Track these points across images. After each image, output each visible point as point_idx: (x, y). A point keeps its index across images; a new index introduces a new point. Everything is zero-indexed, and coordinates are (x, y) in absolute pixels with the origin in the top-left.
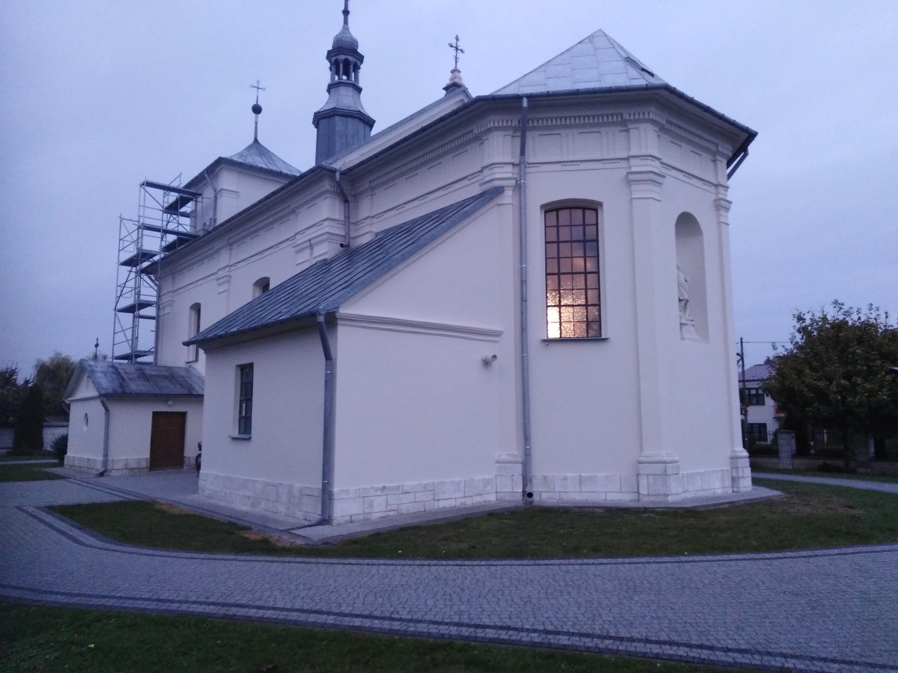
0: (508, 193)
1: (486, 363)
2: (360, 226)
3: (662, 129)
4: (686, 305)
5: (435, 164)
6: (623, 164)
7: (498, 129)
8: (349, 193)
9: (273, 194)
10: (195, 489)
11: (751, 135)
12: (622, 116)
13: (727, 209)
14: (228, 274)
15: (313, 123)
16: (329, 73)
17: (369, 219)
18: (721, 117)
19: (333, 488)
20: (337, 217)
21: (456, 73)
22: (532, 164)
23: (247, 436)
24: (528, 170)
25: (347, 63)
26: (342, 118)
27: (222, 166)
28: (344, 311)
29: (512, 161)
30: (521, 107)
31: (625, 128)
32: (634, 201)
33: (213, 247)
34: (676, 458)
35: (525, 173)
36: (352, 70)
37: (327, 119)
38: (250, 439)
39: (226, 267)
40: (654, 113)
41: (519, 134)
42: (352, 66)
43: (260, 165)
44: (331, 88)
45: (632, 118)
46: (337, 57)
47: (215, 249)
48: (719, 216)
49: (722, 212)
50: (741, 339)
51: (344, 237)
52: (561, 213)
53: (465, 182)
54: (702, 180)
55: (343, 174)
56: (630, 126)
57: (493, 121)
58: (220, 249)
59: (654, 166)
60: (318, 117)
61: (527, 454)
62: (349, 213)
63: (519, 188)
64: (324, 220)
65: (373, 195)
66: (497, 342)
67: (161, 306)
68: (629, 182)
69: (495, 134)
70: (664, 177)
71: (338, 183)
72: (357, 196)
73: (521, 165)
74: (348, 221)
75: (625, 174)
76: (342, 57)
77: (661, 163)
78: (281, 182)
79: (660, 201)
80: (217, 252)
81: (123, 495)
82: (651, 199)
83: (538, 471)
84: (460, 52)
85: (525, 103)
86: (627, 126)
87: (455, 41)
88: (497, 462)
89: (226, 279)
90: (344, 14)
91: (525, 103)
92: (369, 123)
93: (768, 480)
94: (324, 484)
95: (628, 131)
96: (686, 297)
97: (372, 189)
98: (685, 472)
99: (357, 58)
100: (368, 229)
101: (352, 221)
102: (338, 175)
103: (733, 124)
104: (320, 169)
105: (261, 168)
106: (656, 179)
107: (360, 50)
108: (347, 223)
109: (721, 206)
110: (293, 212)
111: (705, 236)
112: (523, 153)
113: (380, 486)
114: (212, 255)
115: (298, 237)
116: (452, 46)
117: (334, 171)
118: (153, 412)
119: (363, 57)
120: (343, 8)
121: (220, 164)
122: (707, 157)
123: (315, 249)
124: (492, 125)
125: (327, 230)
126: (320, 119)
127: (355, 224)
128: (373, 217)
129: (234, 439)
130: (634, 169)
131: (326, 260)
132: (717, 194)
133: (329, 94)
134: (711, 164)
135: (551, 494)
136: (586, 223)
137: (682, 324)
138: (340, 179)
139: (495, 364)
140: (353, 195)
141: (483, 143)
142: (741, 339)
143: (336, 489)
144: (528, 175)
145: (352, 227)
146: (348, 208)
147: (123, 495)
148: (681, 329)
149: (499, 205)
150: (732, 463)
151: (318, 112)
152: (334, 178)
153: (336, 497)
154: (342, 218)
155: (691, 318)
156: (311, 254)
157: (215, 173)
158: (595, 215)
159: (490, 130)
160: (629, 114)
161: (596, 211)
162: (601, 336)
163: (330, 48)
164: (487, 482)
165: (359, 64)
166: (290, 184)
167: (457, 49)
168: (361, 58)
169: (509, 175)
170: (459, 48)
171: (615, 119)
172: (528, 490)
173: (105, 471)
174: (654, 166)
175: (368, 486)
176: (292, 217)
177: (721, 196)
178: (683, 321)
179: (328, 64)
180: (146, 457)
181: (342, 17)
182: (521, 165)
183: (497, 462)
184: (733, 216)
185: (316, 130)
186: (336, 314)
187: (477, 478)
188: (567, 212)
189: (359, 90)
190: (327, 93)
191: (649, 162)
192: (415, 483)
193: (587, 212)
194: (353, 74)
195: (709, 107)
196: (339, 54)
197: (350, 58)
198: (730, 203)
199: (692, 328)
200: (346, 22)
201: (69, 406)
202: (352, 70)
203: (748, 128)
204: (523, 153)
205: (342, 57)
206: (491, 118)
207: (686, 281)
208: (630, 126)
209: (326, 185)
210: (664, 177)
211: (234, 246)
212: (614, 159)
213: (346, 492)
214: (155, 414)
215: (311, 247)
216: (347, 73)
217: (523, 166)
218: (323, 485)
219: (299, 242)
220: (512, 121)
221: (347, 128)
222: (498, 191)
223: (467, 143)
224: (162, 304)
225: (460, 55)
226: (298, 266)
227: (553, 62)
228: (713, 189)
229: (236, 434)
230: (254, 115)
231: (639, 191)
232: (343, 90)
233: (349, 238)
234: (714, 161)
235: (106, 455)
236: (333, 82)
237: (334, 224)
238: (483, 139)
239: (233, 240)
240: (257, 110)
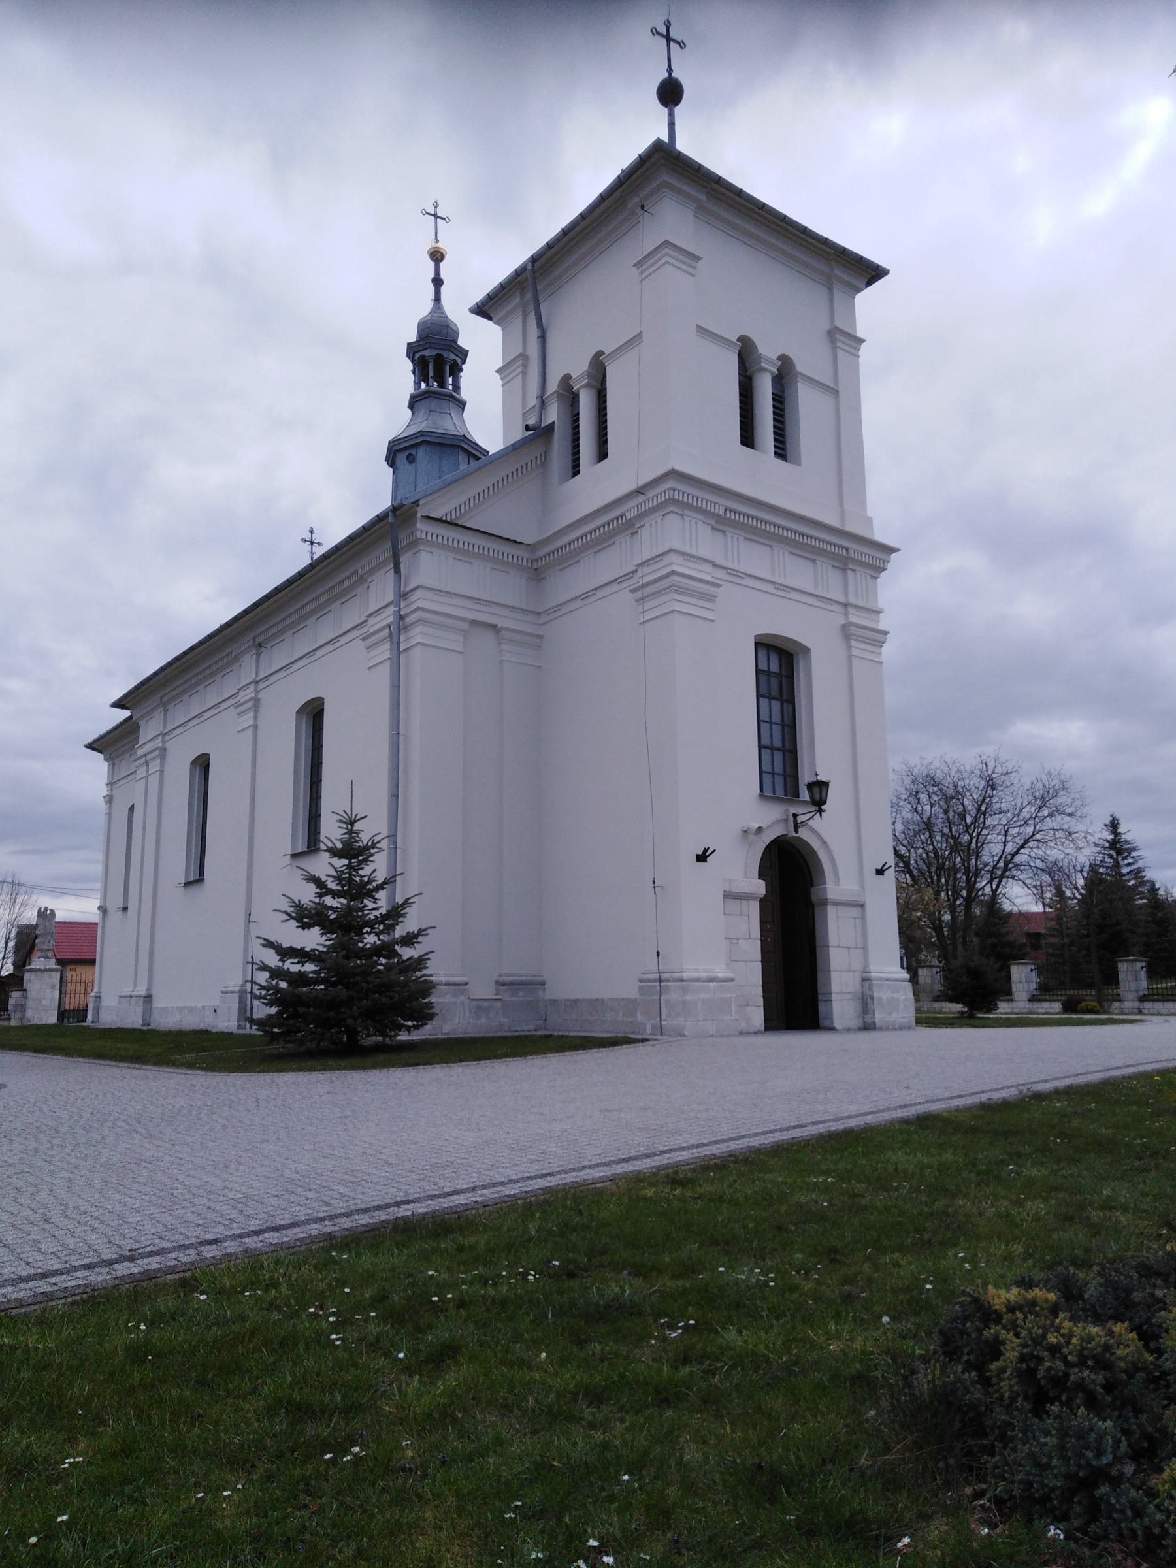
15: (387, 460)
16: (412, 377)
25: (439, 361)
33: (231, 652)
34: (464, 979)
39: (250, 684)
47: (234, 654)
60: (395, 449)
70: (719, 586)
114: (230, 663)
115: (371, 621)
120: (432, 275)
132: (846, 614)
156: (147, 771)
165: (460, 363)
168: (464, 354)
176: (361, 589)
179: (409, 365)
185: (391, 470)
190: (409, 411)
200: (437, 298)
210: (719, 586)
211: (170, 707)
214: (96, 924)
226: (241, 734)
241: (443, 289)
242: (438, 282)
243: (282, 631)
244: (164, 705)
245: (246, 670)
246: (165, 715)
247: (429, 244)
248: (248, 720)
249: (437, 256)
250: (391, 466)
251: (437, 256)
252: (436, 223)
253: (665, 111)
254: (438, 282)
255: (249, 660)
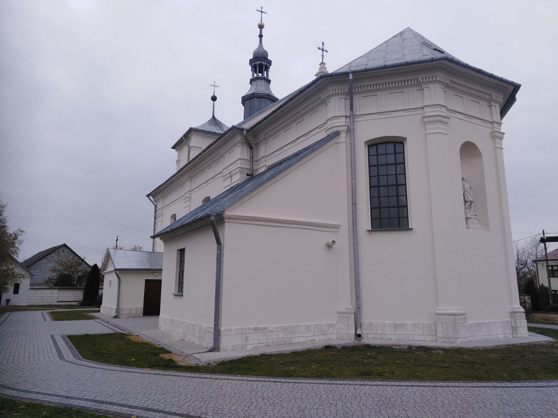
0: (343, 135)
1: (329, 246)
2: (260, 162)
3: (447, 86)
4: (471, 204)
5: (299, 121)
6: (420, 111)
7: (336, 95)
8: (253, 142)
9: (210, 146)
10: (156, 327)
11: (517, 87)
12: (417, 80)
13: (502, 138)
14: (189, 196)
15: (242, 103)
16: (251, 72)
17: (264, 158)
18: (491, 76)
19: (221, 327)
20: (245, 157)
21: (323, 65)
22: (358, 115)
23: (181, 294)
24: (356, 120)
25: (261, 66)
26: (258, 99)
27: (192, 132)
28: (228, 213)
29: (345, 114)
30: (348, 80)
31: (421, 88)
32: (427, 135)
33: (182, 180)
34: (463, 312)
35: (354, 122)
36: (264, 70)
37: (250, 100)
38: (182, 295)
39: (188, 192)
40: (440, 76)
41: (349, 97)
42: (264, 68)
43: (214, 131)
44: (252, 81)
45: (424, 80)
46: (256, 63)
47: (183, 181)
48: (495, 143)
49: (497, 141)
50: (543, 231)
51: (250, 169)
52: (379, 146)
53: (318, 130)
54: (481, 119)
55: (247, 131)
56: (423, 86)
57: (331, 90)
58: (186, 181)
59: (443, 112)
60: (244, 99)
61: (358, 307)
62: (252, 155)
63: (350, 131)
64: (237, 160)
65: (266, 143)
66: (336, 232)
67: (157, 217)
68: (425, 123)
69: (334, 98)
70: (449, 118)
71: (245, 136)
72: (257, 144)
73: (352, 116)
74: (252, 160)
75: (421, 118)
76: (259, 62)
77: (447, 109)
78: (215, 138)
79: (447, 134)
80: (184, 183)
81: (115, 328)
82: (439, 134)
83: (366, 320)
84: (325, 52)
85: (351, 77)
86: (422, 87)
87: (322, 45)
88: (338, 313)
89: (188, 199)
90: (260, 37)
91: (351, 77)
92: (279, 99)
93: (544, 329)
94: (215, 325)
95: (423, 89)
96: (471, 199)
97: (265, 139)
98: (103, 305)
99: (267, 63)
100: (264, 164)
101: (254, 160)
102: (245, 132)
103: (501, 80)
104: (234, 129)
105: (215, 133)
106: (443, 120)
107: (269, 58)
108: (251, 160)
109: (497, 136)
110: (222, 156)
111: (483, 157)
112: (352, 109)
113: (253, 327)
114: (182, 185)
115: (225, 171)
116: (320, 49)
117: (243, 130)
118: (146, 280)
119: (271, 61)
120: (259, 34)
121: (191, 130)
122: (484, 104)
123: (233, 178)
124: (331, 93)
125: (239, 166)
126: (245, 100)
127: (257, 161)
128: (266, 156)
129: (175, 295)
130: (427, 114)
131: (239, 184)
132: (493, 128)
133: (251, 85)
134: (488, 108)
135: (375, 335)
136: (397, 152)
137: (467, 219)
138: (246, 134)
139: (335, 246)
140: (256, 144)
141: (327, 105)
142: (543, 231)
143: (222, 329)
144: (356, 123)
145: (255, 163)
146: (252, 151)
147: (115, 328)
148: (467, 222)
149: (337, 143)
150: (511, 316)
151: (244, 96)
152: (243, 133)
153: (222, 333)
154: (249, 158)
155: (475, 214)
156: (231, 181)
157: (189, 137)
158: (402, 146)
159: (330, 96)
160: (423, 79)
161: (403, 143)
162: (409, 227)
163: (252, 58)
164: (330, 326)
165: (268, 66)
166: (219, 139)
167: (323, 50)
168: (270, 62)
169: (344, 124)
170: (324, 49)
171: (413, 83)
172: (359, 332)
173: (117, 315)
174: (443, 112)
175: (245, 327)
176: (222, 159)
177: (495, 129)
178: (469, 216)
179: (250, 68)
180: (141, 307)
181: (258, 39)
182: (352, 116)
183: (338, 313)
184: (506, 143)
185: (244, 107)
186: (223, 215)
187: (323, 323)
188: (383, 146)
189: (269, 81)
190: (250, 85)
191: (438, 109)
192: (279, 325)
193: (397, 145)
194: (265, 72)
195: (480, 69)
196: (256, 61)
197: (263, 63)
198: (504, 134)
199: (476, 221)
200: (261, 42)
201: (103, 276)
202: (264, 70)
203: (513, 82)
204: (352, 109)
205: (259, 62)
206: (331, 88)
207: (470, 188)
208: (423, 86)
209: (238, 138)
210: (449, 118)
211: (193, 179)
212: (413, 109)
213: (230, 330)
214: (147, 281)
215: (231, 177)
216: (261, 72)
217: (352, 117)
218: (214, 325)
219: (225, 174)
220: (344, 89)
221: (261, 104)
222: (337, 134)
223: (317, 106)
224: (157, 215)
225: (325, 53)
227: (373, 51)
228: (489, 125)
229: (177, 293)
230: (213, 102)
231: (431, 128)
232: (259, 82)
233: (253, 170)
234: (490, 106)
235: (118, 305)
236: (254, 77)
237: (244, 162)
238: (327, 102)
239: (192, 175)
240: (214, 99)
241: (263, 39)
242: (261, 36)
243: (212, 163)
244: (191, 178)
245: (187, 187)
246: (191, 183)
247: (258, 22)
248: (188, 204)
249: (261, 27)
250: (244, 106)
251: (261, 27)
252: (262, 14)
253: (266, 47)
254: (261, 36)
255: (188, 184)
